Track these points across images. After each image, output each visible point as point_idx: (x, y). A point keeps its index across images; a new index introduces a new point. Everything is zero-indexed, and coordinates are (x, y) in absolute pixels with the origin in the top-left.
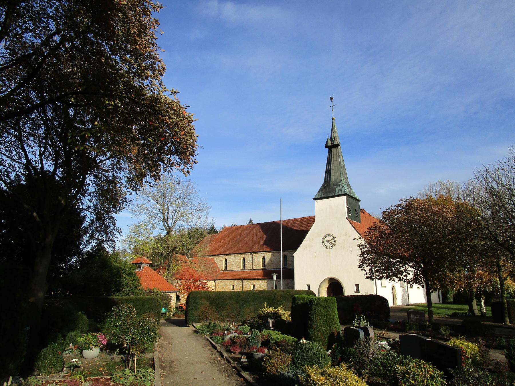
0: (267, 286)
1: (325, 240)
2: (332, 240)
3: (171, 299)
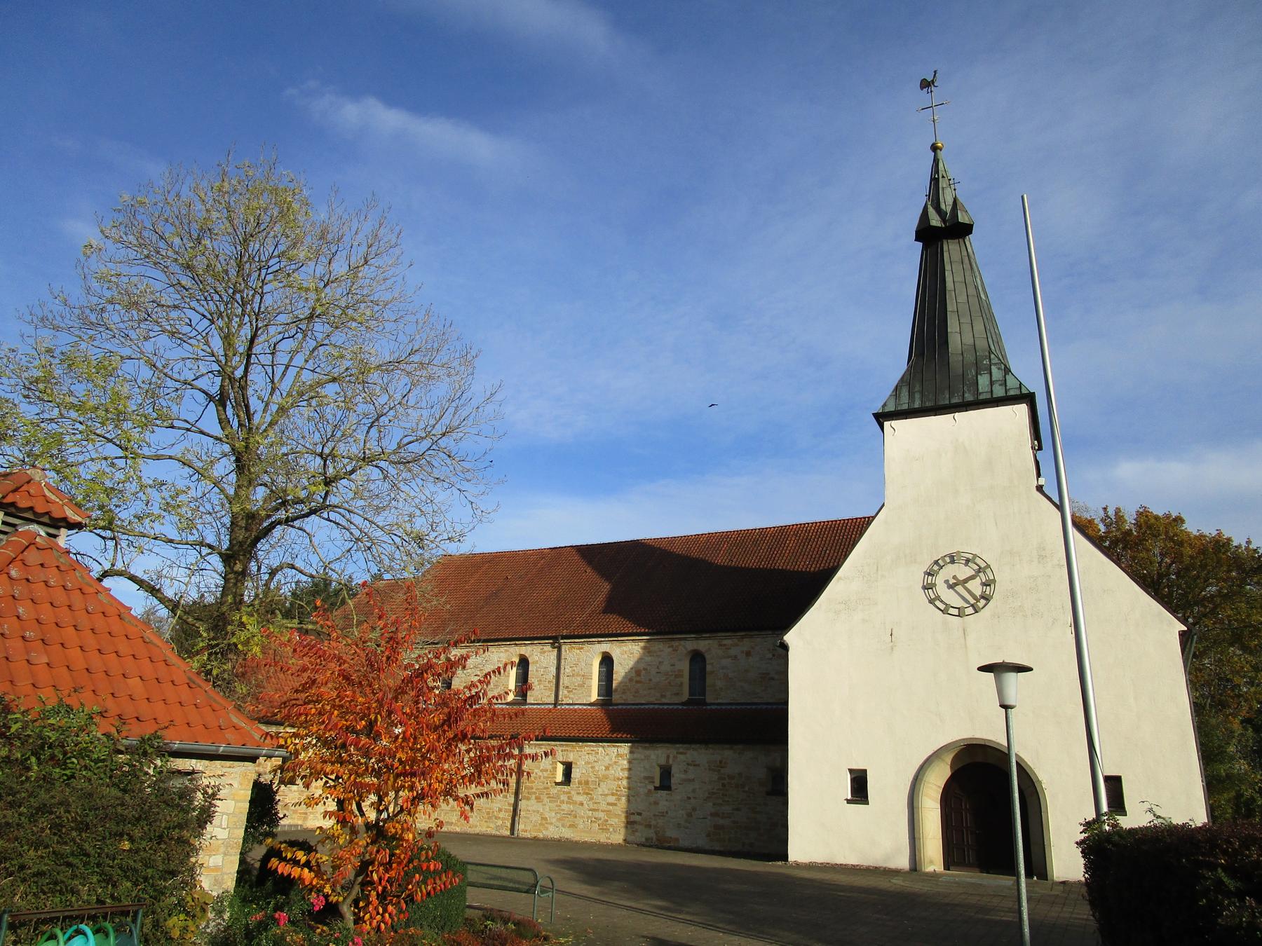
0: (630, 769)
1: (939, 580)
2: (972, 578)
3: (206, 816)
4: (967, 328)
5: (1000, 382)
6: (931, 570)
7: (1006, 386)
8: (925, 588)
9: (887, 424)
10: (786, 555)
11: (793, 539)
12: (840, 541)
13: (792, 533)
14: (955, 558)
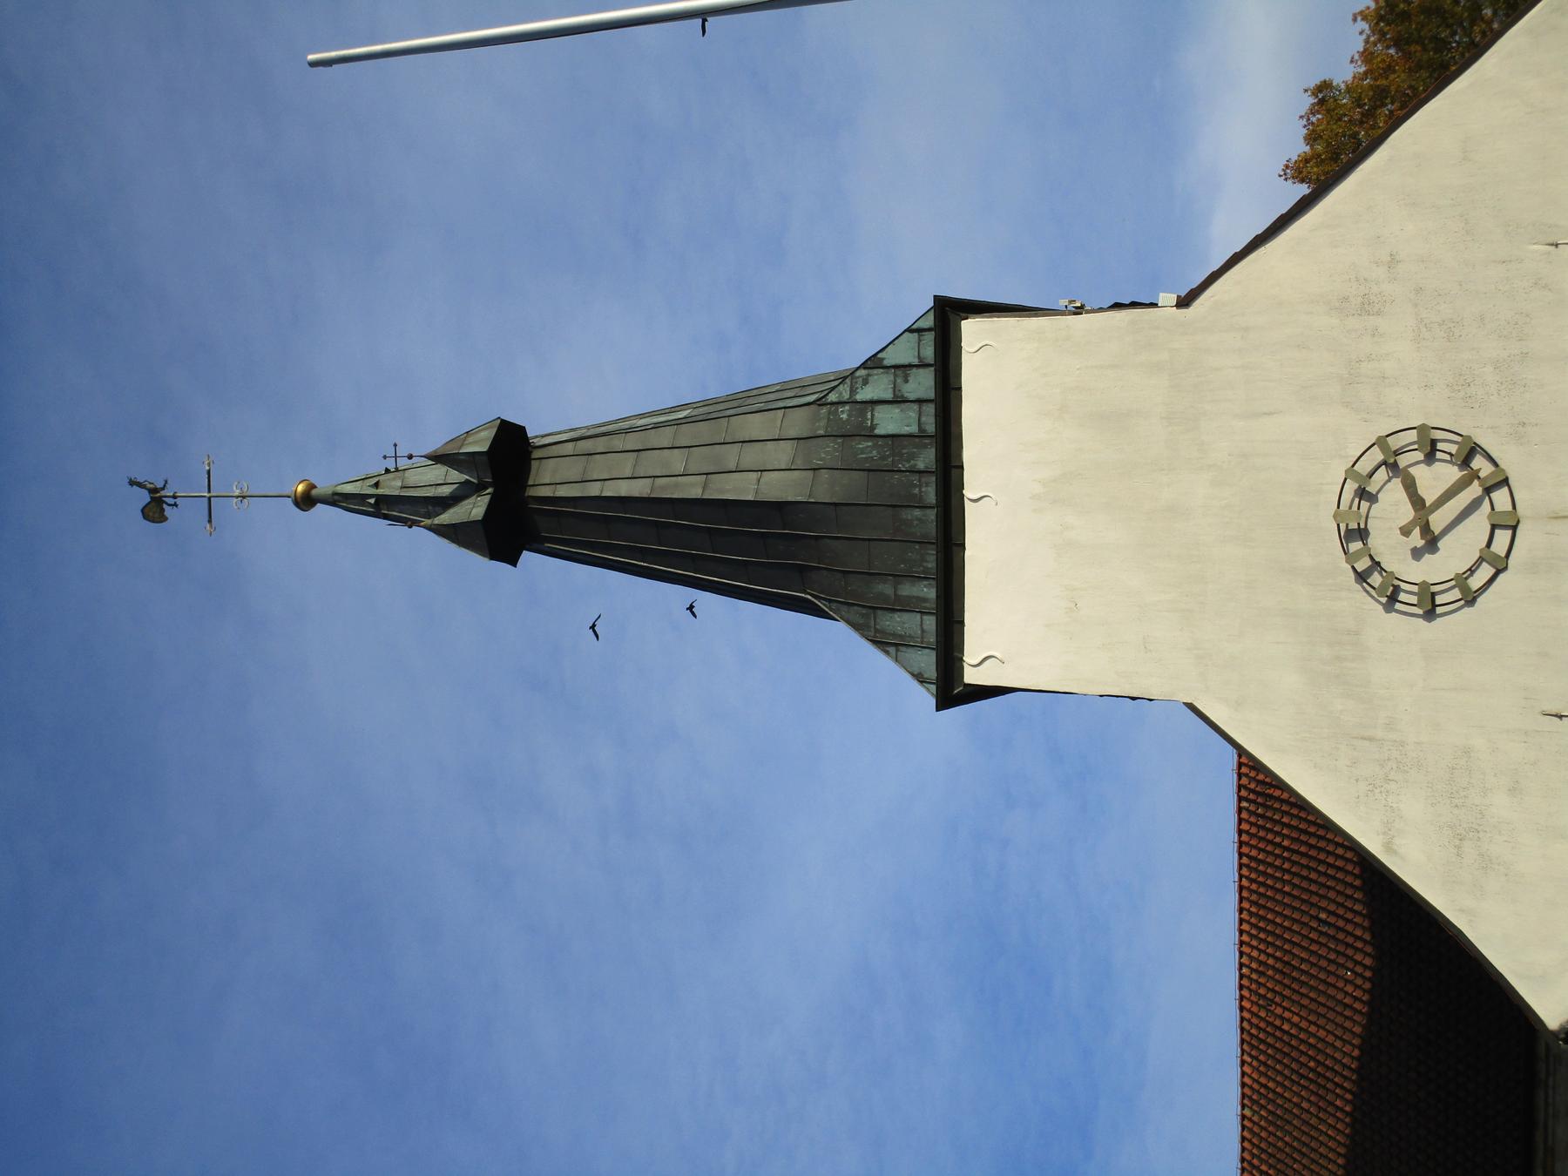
2: (1410, 486)
4: (751, 456)
5: (899, 381)
6: (1380, 591)
7: (910, 366)
8: (1430, 614)
9: (971, 676)
10: (1322, 1033)
11: (1279, 1011)
12: (1296, 881)
13: (1263, 1014)
14: (1353, 526)
